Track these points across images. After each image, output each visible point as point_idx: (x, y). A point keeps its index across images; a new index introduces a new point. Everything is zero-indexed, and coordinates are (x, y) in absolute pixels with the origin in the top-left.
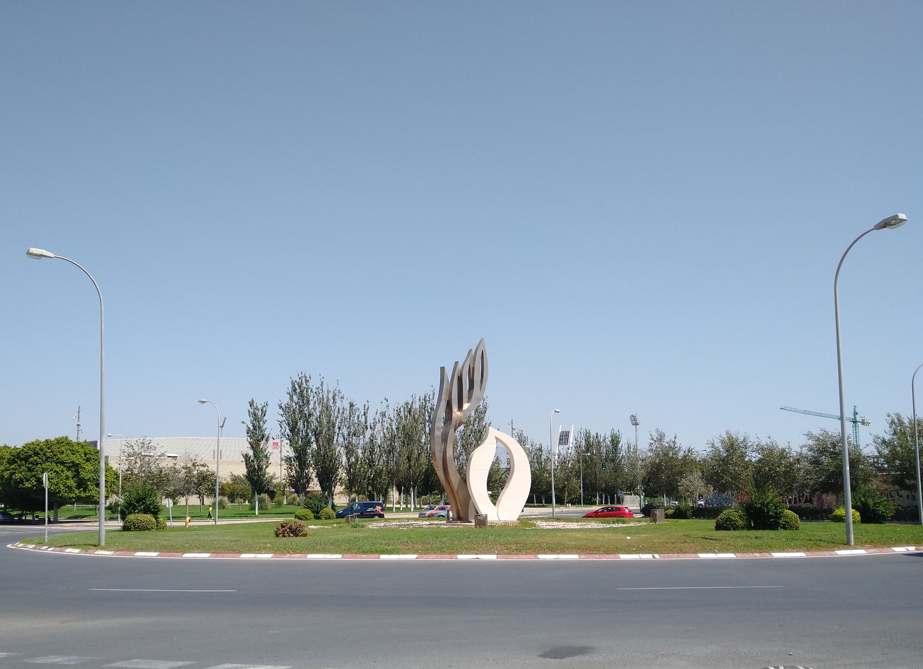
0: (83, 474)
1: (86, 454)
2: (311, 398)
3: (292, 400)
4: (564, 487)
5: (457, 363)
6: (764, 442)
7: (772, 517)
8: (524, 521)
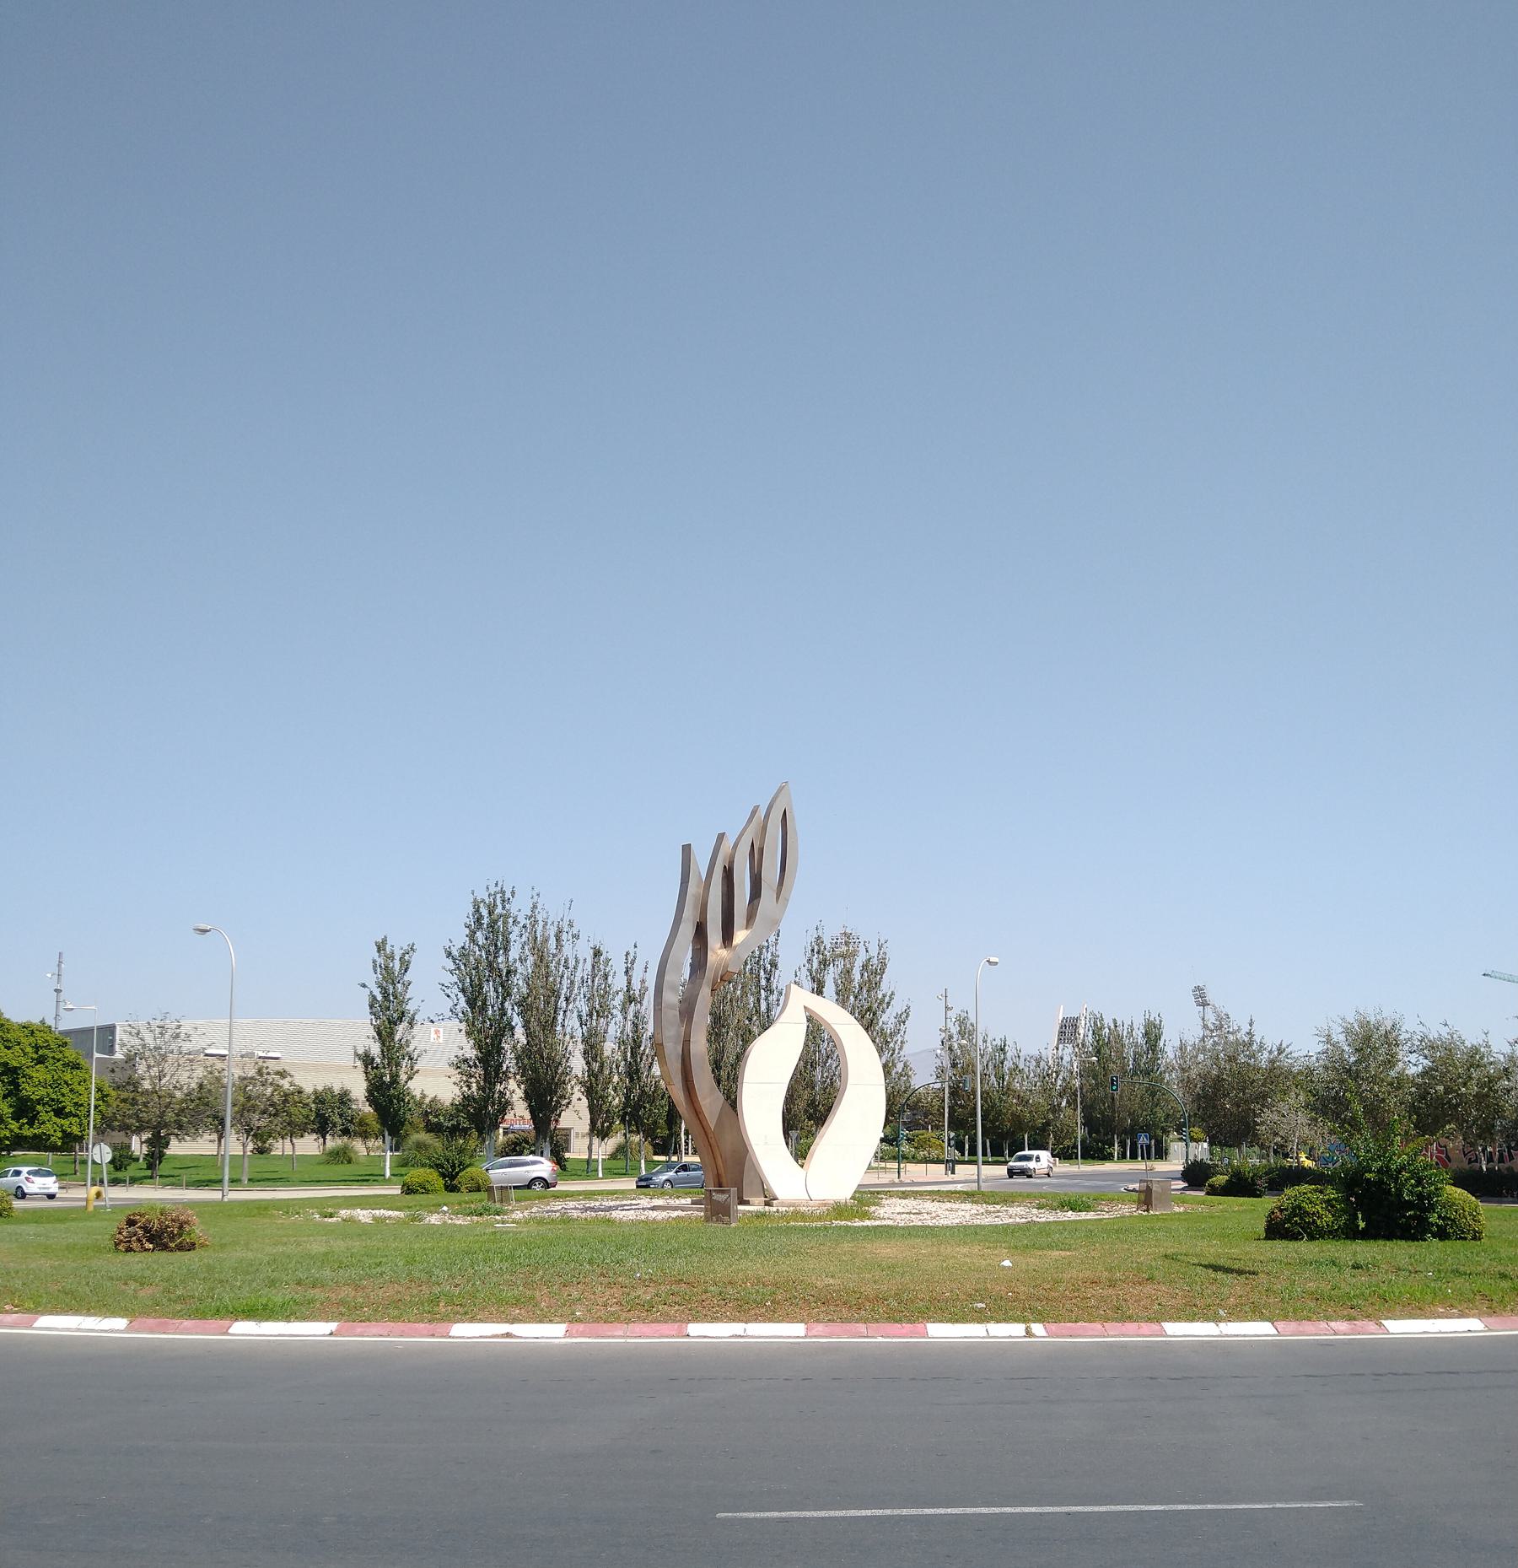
0: (27, 1090)
1: (37, 1048)
2: (513, 937)
3: (473, 940)
4: (1048, 1124)
5: (721, 837)
6: (1436, 1031)
7: (1409, 1205)
8: (866, 1197)
